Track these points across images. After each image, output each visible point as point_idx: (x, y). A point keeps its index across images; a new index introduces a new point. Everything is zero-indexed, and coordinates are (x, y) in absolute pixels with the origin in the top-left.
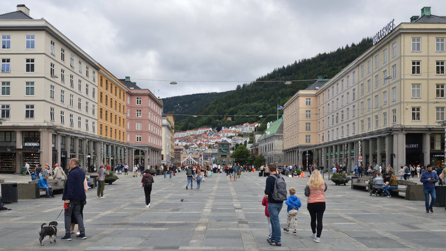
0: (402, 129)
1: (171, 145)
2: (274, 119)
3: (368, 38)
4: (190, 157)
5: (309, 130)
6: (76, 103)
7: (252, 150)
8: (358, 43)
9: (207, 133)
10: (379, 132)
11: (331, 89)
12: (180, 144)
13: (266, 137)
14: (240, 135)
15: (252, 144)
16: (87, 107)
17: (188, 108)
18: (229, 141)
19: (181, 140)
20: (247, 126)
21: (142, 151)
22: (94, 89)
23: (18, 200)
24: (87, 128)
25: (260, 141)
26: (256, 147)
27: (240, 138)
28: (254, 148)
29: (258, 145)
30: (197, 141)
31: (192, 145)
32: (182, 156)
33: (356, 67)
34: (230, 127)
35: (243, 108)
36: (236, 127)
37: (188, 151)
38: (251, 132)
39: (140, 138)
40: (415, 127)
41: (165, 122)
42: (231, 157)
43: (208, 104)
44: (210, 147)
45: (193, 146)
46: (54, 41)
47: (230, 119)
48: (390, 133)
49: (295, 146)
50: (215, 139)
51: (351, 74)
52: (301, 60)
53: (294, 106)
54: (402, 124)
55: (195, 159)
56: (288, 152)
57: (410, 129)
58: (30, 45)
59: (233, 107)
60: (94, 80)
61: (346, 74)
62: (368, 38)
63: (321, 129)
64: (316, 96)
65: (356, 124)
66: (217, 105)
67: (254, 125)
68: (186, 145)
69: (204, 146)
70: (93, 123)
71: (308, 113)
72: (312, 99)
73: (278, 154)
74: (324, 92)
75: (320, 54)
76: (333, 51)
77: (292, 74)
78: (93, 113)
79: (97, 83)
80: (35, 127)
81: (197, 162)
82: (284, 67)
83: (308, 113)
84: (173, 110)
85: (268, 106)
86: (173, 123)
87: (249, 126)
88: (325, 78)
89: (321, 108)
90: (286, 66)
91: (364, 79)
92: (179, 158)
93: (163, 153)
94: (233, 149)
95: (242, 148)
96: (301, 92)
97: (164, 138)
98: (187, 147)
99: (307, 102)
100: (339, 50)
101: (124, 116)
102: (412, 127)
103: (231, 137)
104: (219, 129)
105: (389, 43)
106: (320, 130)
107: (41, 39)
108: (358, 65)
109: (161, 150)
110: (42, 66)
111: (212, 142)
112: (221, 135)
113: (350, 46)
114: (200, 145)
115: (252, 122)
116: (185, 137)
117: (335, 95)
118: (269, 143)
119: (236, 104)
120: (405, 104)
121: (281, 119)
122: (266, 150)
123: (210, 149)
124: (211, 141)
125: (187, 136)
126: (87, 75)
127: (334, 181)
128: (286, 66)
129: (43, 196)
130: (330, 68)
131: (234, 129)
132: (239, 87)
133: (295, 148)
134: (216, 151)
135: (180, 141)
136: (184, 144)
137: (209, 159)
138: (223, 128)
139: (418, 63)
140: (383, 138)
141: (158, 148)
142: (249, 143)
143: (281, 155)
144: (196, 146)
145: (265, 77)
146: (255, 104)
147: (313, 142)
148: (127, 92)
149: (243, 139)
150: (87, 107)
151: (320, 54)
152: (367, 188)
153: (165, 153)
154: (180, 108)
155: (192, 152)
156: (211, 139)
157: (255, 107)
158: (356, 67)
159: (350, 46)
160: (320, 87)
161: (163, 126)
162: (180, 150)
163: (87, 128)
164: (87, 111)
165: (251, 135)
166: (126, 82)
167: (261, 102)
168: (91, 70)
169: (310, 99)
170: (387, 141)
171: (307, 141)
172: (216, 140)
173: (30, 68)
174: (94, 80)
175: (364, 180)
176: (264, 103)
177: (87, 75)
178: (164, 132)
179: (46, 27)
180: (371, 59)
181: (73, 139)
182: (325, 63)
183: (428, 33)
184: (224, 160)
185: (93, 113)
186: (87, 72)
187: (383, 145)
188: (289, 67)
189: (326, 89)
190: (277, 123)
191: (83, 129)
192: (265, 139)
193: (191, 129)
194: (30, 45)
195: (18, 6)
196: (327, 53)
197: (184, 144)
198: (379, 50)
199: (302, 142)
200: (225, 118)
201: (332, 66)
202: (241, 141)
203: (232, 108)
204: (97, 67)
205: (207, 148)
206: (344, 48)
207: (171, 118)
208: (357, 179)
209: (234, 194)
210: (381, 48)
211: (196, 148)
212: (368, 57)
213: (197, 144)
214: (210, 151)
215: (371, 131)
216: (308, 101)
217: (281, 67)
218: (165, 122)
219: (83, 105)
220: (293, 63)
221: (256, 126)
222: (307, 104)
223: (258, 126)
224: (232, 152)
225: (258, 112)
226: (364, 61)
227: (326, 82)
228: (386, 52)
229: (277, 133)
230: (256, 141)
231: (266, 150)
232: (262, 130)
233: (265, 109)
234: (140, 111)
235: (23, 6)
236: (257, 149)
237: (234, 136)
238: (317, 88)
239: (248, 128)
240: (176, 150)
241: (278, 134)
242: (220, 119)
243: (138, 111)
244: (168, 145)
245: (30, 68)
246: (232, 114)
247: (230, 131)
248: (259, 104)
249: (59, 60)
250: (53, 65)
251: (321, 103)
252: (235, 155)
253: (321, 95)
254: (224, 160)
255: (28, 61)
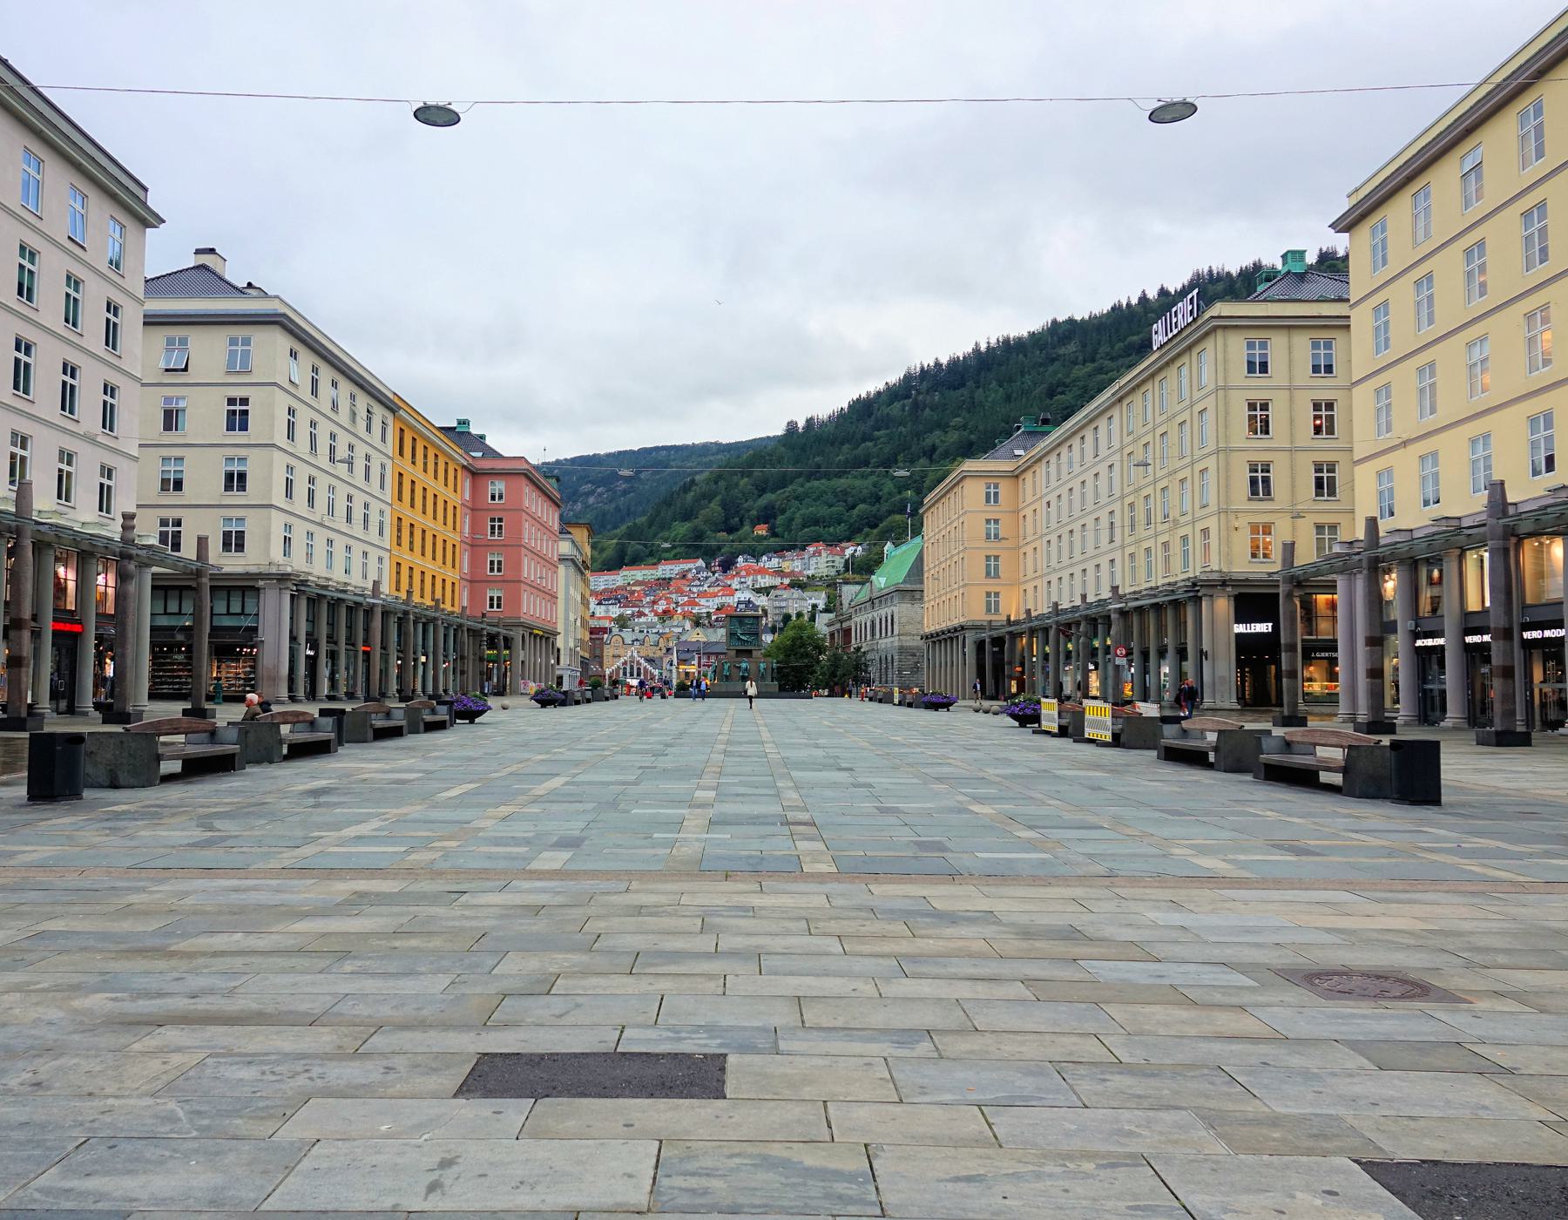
0: (1224, 583)
1: (582, 618)
2: (899, 538)
3: (1210, 271)
4: (633, 652)
5: (997, 576)
6: (301, 489)
7: (832, 635)
8: (1179, 287)
9: (690, 576)
10: (1172, 588)
11: (1053, 458)
12: (600, 611)
13: (875, 595)
14: (797, 585)
15: (832, 616)
16: (311, 493)
17: (625, 492)
18: (761, 601)
19: (606, 597)
20: (818, 553)
21: (506, 639)
22: (383, 466)
23: (86, 793)
24: (309, 556)
25: (858, 607)
26: (845, 625)
27: (796, 593)
28: (838, 626)
29: (850, 618)
30: (654, 602)
31: (641, 614)
32: (608, 651)
33: (1113, 404)
34: (765, 558)
35: (807, 495)
36: (782, 557)
37: (628, 635)
38: (833, 572)
39: (499, 563)
40: (1258, 576)
41: (565, 548)
42: (768, 655)
43: (693, 482)
44: (697, 623)
45: (642, 619)
46: (298, 347)
47: (761, 530)
48: (1198, 591)
49: (956, 622)
50: (715, 595)
51: (1102, 423)
52: (993, 341)
53: (1053, 468)
54: (1125, 589)
55: (650, 661)
56: (936, 639)
57: (1246, 582)
58: (239, 365)
59: (773, 491)
60: (335, 406)
61: (1091, 421)
62: (1210, 271)
63: (1030, 574)
64: (1016, 476)
65: (1118, 563)
66: (722, 484)
67: (843, 550)
68: (621, 616)
69: (677, 619)
70: (380, 559)
71: (992, 526)
72: (1004, 488)
73: (911, 648)
74: (1036, 468)
75: (1054, 322)
76: (1097, 311)
77: (964, 385)
78: (381, 533)
79: (391, 446)
80: (248, 576)
81: (656, 672)
82: (938, 364)
83: (992, 526)
84: (575, 502)
85: (886, 490)
86: (588, 550)
87: (824, 554)
88: (1045, 422)
89: (1028, 512)
90: (944, 361)
91: (1169, 419)
92: (599, 658)
93: (560, 643)
94: (773, 630)
95: (801, 628)
96: (969, 465)
97: (561, 596)
98: (622, 622)
99: (988, 494)
100: (1116, 309)
101: (454, 538)
102: (1251, 577)
103: (765, 591)
104: (727, 566)
105: (1189, 348)
106: (1102, 550)
107: (271, 347)
108: (1120, 400)
109: (556, 634)
110: (267, 416)
111: (708, 605)
112: (735, 584)
113: (1152, 294)
114: (666, 615)
115: (833, 542)
116: (619, 588)
117: (1065, 477)
118: (883, 612)
119: (783, 482)
120: (1232, 517)
121: (918, 539)
122: (873, 634)
123: (698, 630)
124: (703, 601)
125: (623, 588)
126: (315, 392)
127: (1014, 716)
128: (944, 361)
129: (170, 778)
130: (1090, 367)
131: (775, 562)
132: (792, 427)
133: (956, 630)
134: (720, 635)
135: (600, 604)
136: (615, 611)
137: (695, 662)
138: (740, 559)
139: (1265, 407)
140: (1176, 604)
141: (548, 627)
142: (827, 610)
143: (918, 648)
144: (652, 618)
145: (879, 393)
146: (842, 483)
147: (1012, 607)
148: (464, 467)
149: (806, 594)
150: (311, 493)
151: (1054, 322)
152: (1212, 758)
153: (566, 642)
154: (600, 495)
155: (641, 637)
156: (702, 595)
157: (845, 493)
158: (1113, 404)
159: (1152, 294)
160: (1025, 449)
161: (562, 560)
162: (604, 630)
163: (309, 556)
164: (366, 528)
165: (831, 585)
166: (459, 434)
167: (864, 477)
168: (379, 412)
169: (996, 486)
170: (1190, 611)
171: (989, 610)
172: (718, 601)
173: (238, 418)
174: (335, 406)
175: (1315, 745)
176: (873, 478)
177: (315, 392)
178: (564, 581)
179: (284, 315)
180: (1149, 386)
181: (335, 604)
182: (1072, 348)
183: (1289, 327)
184: (744, 665)
185: (381, 533)
186: (315, 382)
187: (1180, 625)
188: (954, 363)
189: (1040, 460)
190: (909, 549)
191: (338, 575)
192: (871, 600)
193: (635, 561)
194: (239, 365)
195: (198, 252)
196: (1078, 318)
197: (615, 611)
198: (1167, 364)
199: (976, 612)
200: (747, 528)
201: (1093, 360)
202: (798, 603)
203: (769, 497)
204: (391, 405)
205: (688, 625)
206: (1134, 301)
207: (581, 535)
208: (1176, 726)
209: (766, 735)
210: (1173, 360)
211: (651, 625)
212: (1144, 382)
213: (656, 614)
214: (697, 636)
215: (1153, 584)
216: (992, 490)
217: (929, 361)
218: (565, 548)
219: (358, 514)
220: (969, 349)
221: (848, 552)
222: (988, 500)
223: (853, 555)
224: (768, 638)
225: (853, 507)
226: (1133, 389)
227: (1046, 433)
228: (1208, 356)
229: (905, 582)
230: (846, 605)
231: (873, 634)
232: (864, 568)
233: (878, 499)
234: (500, 520)
235: (212, 251)
236: (847, 632)
237: (774, 587)
238: (1017, 452)
239: (819, 562)
240: (593, 631)
241: (909, 587)
242: (730, 531)
243: (493, 520)
244: (572, 618)
245: (238, 418)
246: (767, 516)
247: (763, 571)
248: (858, 483)
249: (308, 397)
250: (116, 308)
251: (1029, 499)
252: (778, 648)
253: (1028, 476)
254: (744, 665)
255: (231, 401)
